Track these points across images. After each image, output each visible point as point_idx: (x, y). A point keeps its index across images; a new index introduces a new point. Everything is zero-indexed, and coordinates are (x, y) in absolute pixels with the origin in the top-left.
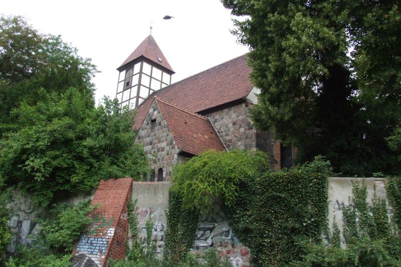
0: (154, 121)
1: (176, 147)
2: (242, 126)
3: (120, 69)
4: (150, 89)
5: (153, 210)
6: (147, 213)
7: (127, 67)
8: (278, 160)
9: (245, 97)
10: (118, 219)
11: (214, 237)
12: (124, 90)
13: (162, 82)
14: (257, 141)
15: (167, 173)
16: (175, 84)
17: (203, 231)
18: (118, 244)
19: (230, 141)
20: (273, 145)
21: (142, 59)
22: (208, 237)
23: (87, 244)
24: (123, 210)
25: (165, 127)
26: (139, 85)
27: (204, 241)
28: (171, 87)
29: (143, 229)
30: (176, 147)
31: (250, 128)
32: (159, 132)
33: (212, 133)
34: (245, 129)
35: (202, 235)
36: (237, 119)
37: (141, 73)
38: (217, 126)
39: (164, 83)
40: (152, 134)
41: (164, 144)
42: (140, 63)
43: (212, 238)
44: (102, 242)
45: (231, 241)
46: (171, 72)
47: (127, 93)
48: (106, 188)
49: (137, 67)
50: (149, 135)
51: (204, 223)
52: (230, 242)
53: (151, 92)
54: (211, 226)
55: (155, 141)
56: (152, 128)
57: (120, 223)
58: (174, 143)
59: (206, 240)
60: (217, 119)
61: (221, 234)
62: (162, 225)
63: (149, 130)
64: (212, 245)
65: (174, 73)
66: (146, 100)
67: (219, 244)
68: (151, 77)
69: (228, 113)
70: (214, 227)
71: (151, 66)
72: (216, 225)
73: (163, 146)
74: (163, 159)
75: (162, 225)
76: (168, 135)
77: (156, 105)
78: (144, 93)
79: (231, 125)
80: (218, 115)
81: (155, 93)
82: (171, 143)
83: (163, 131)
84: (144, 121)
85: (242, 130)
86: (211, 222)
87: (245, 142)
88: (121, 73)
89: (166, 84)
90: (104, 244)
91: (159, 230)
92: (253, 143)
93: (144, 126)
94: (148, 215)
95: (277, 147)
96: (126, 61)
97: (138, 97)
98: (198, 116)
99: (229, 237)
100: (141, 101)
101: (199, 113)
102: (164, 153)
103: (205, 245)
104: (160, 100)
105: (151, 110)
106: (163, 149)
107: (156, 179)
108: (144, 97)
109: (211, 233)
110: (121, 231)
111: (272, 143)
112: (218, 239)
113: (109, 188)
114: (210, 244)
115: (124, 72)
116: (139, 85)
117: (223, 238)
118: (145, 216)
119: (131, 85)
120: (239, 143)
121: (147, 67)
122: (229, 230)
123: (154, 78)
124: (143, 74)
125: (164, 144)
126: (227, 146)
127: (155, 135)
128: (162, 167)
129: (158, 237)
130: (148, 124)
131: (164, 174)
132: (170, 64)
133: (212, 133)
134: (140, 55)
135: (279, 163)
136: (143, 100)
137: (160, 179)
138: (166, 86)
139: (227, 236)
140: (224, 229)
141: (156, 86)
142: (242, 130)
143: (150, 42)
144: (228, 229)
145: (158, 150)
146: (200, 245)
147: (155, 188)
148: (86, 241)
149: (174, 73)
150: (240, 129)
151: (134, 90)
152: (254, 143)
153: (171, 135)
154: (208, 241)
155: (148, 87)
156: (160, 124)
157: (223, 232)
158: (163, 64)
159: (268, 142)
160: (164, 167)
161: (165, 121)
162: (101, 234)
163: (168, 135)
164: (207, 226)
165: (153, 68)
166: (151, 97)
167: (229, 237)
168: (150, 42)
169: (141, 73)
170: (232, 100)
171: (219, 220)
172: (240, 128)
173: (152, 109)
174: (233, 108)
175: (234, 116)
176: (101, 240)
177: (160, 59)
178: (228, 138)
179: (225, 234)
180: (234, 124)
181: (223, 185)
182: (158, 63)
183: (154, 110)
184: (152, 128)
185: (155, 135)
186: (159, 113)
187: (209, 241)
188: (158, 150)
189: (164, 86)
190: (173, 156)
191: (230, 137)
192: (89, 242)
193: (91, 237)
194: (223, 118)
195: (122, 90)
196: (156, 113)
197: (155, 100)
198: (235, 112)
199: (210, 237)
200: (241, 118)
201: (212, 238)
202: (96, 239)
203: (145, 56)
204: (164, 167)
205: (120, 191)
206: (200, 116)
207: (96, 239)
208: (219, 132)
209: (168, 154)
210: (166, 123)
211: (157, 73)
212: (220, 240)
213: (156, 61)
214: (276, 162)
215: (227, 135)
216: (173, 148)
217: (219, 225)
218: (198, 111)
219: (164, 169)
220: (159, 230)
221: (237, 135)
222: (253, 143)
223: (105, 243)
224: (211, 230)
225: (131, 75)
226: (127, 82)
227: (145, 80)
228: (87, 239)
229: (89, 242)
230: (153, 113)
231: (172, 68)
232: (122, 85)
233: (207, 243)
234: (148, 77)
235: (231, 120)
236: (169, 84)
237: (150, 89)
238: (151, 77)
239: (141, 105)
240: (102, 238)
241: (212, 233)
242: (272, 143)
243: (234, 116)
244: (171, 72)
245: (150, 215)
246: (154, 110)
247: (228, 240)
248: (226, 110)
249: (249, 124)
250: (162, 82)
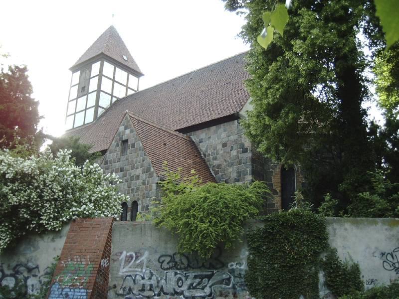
0: (125, 142)
1: (155, 175)
2: (234, 148)
3: (74, 69)
4: (112, 96)
5: (139, 255)
6: (132, 258)
7: (83, 66)
8: (278, 190)
9: (238, 113)
10: (98, 266)
11: (213, 285)
12: (78, 97)
13: (127, 87)
14: (253, 167)
15: (143, 207)
16: (141, 92)
17: (200, 278)
18: (98, 296)
19: (219, 166)
20: (272, 172)
21: (103, 57)
22: (206, 286)
23: (61, 296)
24: (103, 255)
25: (140, 150)
26: (99, 91)
27: (201, 291)
28: (138, 95)
29: (128, 277)
30: (155, 175)
31: (245, 151)
32: (130, 154)
33: (196, 156)
34: (238, 152)
35: (199, 284)
36: (227, 140)
37: (101, 75)
38: (202, 147)
39: (130, 88)
40: (123, 158)
41: (139, 171)
42: (100, 62)
43: (210, 287)
44: (80, 294)
45: (232, 290)
46: (137, 74)
47: (82, 100)
48: (81, 229)
49: (95, 68)
50: (119, 159)
51: (201, 270)
52: (231, 291)
53: (114, 100)
54: (210, 273)
55: (127, 167)
56: (124, 151)
57: (101, 271)
58: (152, 169)
59: (203, 289)
60: (202, 139)
61: (221, 282)
62: (151, 273)
63: (119, 153)
64: (210, 295)
65: (143, 75)
66: (107, 110)
67: (218, 293)
68: (114, 81)
69: (216, 132)
70: (213, 274)
71: (113, 67)
72: (215, 272)
73: (137, 174)
74: (138, 189)
75: (151, 273)
76: (143, 161)
77: (129, 122)
78: (105, 102)
79: (220, 147)
80: (204, 134)
81: (119, 101)
82: (148, 170)
83: (138, 155)
84: (112, 141)
85: (234, 153)
86: (209, 268)
87: (238, 169)
88: (74, 74)
89: (134, 90)
90: (83, 296)
91: (146, 278)
92: (248, 169)
93: (113, 147)
94: (133, 261)
95: (276, 174)
96: (80, 59)
97: (97, 106)
98: (179, 135)
99: (231, 286)
100: (100, 111)
101: (180, 131)
102: (139, 182)
103: (203, 294)
104: (133, 116)
105: (122, 128)
106: (138, 177)
107: (128, 218)
108: (105, 107)
109: (208, 281)
110: (101, 280)
111: (271, 170)
112: (217, 288)
113: (84, 229)
114: (208, 294)
115: (79, 73)
116: (99, 91)
117: (223, 286)
118: (130, 262)
119: (88, 91)
120: (230, 170)
121: (108, 68)
122: (230, 277)
123: (117, 82)
124: (103, 77)
125: (139, 171)
126: (214, 173)
127: (127, 159)
128: (136, 199)
129: (146, 286)
130: (117, 145)
131: (140, 207)
132: (137, 63)
133: (196, 156)
134: (100, 52)
135: (280, 194)
136: (104, 111)
137: (124, 219)
138: (133, 92)
139: (229, 285)
140: (224, 276)
141: (120, 93)
142: (234, 153)
143: (111, 36)
144: (228, 276)
145: (132, 178)
146: (196, 295)
147: (141, 229)
148: (60, 292)
149: (143, 75)
150: (232, 152)
151: (92, 98)
152: (249, 170)
153: (148, 160)
154: (206, 290)
155: (126, 85)
156: (133, 146)
157: (223, 280)
158: (129, 64)
159: (265, 168)
160: (139, 199)
161: (140, 142)
162: (78, 284)
163: (143, 161)
164: (204, 273)
165: (117, 69)
166: (113, 106)
167: (231, 286)
168: (111, 36)
169: (101, 75)
170: (220, 116)
171: (218, 266)
172: (231, 151)
173: (123, 127)
174: (222, 125)
175: (224, 135)
176: (78, 290)
177: (125, 58)
178: (216, 163)
179: (226, 282)
180: (224, 145)
181: (227, 226)
182: (123, 62)
183: (126, 128)
184: (124, 151)
185: (127, 159)
186: (132, 132)
187: (207, 290)
188: (132, 178)
189: (130, 92)
190: (151, 186)
191: (218, 161)
192: (64, 293)
193: (65, 288)
194: (210, 137)
195: (76, 97)
196: (128, 131)
197: (127, 115)
198: (225, 131)
199: (208, 285)
200: (232, 138)
201: (210, 287)
202: (72, 290)
203: (107, 53)
204: (139, 199)
205: (98, 233)
206: (181, 135)
207: (72, 290)
208: (205, 155)
209: (144, 184)
210: (141, 145)
211: (121, 75)
212: (220, 289)
213: (120, 60)
214: (275, 192)
215: (215, 159)
216: (151, 176)
217: (218, 272)
218: (178, 128)
219: (139, 202)
220: (146, 278)
221: (228, 159)
222: (248, 169)
223: (83, 294)
224: (209, 277)
225: (88, 77)
226: (83, 86)
227: (106, 85)
228: (60, 290)
229: (64, 293)
230: (124, 132)
231: (140, 68)
232: (75, 92)
233: (205, 292)
234: (110, 80)
235: (220, 141)
236: (136, 90)
237: (112, 96)
238: (114, 81)
239: (102, 116)
240: (80, 289)
241: (210, 281)
242: (271, 170)
243: (224, 135)
244: (137, 74)
245: (135, 260)
246: (126, 128)
247: (229, 288)
248: (213, 128)
249: (242, 146)
250: (127, 87)
